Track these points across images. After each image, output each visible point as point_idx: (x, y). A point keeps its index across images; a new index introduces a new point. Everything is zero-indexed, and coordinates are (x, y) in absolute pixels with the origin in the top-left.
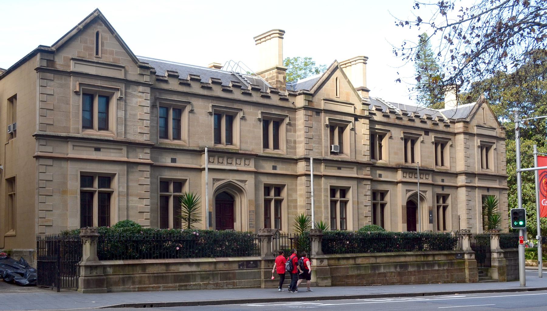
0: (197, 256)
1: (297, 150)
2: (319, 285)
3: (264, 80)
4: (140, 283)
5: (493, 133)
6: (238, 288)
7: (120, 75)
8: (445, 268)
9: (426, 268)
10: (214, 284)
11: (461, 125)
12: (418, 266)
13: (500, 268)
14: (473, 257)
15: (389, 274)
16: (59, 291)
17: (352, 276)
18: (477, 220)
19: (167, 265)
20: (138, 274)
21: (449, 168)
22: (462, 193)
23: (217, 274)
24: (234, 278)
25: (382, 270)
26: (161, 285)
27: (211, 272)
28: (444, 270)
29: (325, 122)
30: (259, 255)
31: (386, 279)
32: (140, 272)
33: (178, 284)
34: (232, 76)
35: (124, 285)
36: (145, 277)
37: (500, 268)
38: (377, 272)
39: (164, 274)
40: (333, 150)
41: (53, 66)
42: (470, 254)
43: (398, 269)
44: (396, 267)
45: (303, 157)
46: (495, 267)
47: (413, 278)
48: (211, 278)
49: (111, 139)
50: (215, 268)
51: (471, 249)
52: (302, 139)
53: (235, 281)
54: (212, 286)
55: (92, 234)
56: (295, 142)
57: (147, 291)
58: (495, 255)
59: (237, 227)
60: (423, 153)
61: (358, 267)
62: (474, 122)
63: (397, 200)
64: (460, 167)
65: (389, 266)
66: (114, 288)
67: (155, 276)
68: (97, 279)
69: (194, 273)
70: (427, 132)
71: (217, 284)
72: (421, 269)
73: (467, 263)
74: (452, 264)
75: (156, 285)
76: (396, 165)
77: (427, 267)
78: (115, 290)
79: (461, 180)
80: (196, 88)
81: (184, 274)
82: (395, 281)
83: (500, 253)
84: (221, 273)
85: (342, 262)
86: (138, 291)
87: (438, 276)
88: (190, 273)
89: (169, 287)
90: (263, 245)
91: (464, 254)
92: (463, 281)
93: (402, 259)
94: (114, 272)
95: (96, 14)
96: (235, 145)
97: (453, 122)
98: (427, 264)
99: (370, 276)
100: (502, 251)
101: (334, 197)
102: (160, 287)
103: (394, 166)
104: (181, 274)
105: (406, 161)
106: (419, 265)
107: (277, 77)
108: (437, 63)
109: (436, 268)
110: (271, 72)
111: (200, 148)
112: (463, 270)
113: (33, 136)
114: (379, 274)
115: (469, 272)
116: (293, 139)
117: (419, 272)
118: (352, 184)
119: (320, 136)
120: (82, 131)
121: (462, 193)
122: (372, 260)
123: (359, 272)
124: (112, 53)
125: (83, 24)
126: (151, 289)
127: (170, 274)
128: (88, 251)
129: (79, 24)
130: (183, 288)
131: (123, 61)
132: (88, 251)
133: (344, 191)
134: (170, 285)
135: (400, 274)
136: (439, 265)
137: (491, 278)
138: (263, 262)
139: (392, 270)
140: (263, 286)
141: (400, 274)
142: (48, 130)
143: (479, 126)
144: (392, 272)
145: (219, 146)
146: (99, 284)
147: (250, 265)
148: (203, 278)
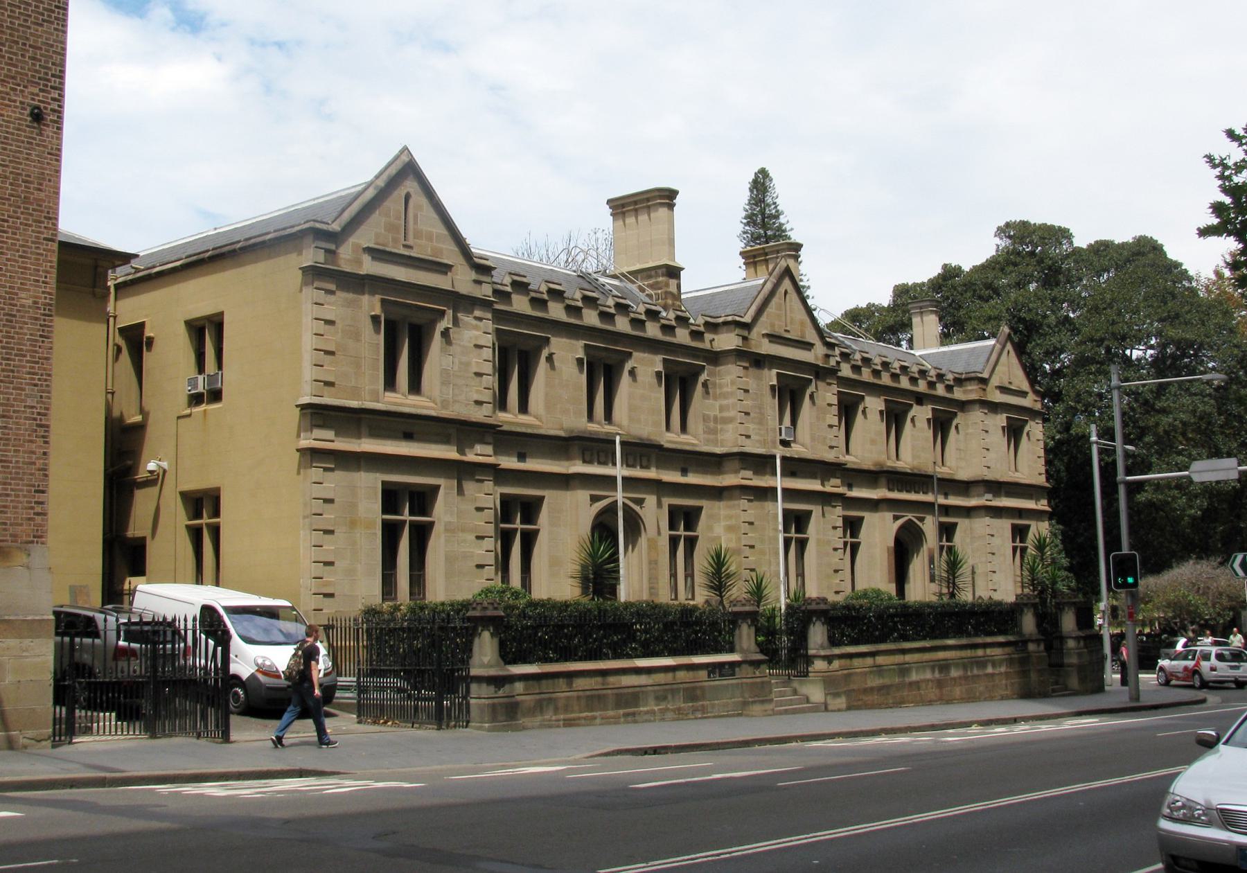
4: (567, 709)
8: (1003, 669)
9: (975, 672)
10: (674, 711)
12: (965, 667)
14: (1042, 647)
15: (923, 685)
16: (439, 728)
17: (872, 689)
19: (604, 673)
20: (561, 691)
23: (678, 689)
24: (703, 698)
25: (914, 677)
26: (596, 714)
30: (732, 650)
32: (564, 688)
33: (621, 712)
34: (580, 280)
38: (907, 680)
41: (334, 263)
43: (937, 675)
46: (1070, 665)
47: (958, 691)
48: (670, 697)
49: (433, 413)
55: (496, 613)
58: (1071, 644)
60: (639, 405)
61: (879, 670)
62: (995, 381)
63: (565, 524)
65: (924, 667)
66: (523, 721)
67: (588, 697)
70: (920, 399)
71: (679, 709)
76: (875, 465)
78: (530, 725)
80: (556, 311)
81: (630, 690)
83: (1077, 639)
84: (684, 689)
85: (857, 662)
86: (565, 726)
93: (941, 655)
94: (526, 688)
95: (405, 158)
97: (713, 327)
98: (977, 662)
99: (900, 687)
100: (1081, 634)
101: (396, 511)
102: (595, 718)
103: (872, 468)
104: (626, 691)
109: (990, 670)
111: (565, 431)
114: (911, 684)
117: (966, 678)
118: (446, 486)
122: (898, 658)
124: (430, 237)
125: (385, 177)
129: (377, 177)
130: (630, 719)
131: (449, 254)
133: (422, 500)
134: (611, 713)
135: (940, 684)
136: (994, 666)
137: (1066, 689)
141: (940, 684)
142: (326, 394)
143: (774, 338)
145: (503, 416)
147: (724, 671)
148: (660, 698)
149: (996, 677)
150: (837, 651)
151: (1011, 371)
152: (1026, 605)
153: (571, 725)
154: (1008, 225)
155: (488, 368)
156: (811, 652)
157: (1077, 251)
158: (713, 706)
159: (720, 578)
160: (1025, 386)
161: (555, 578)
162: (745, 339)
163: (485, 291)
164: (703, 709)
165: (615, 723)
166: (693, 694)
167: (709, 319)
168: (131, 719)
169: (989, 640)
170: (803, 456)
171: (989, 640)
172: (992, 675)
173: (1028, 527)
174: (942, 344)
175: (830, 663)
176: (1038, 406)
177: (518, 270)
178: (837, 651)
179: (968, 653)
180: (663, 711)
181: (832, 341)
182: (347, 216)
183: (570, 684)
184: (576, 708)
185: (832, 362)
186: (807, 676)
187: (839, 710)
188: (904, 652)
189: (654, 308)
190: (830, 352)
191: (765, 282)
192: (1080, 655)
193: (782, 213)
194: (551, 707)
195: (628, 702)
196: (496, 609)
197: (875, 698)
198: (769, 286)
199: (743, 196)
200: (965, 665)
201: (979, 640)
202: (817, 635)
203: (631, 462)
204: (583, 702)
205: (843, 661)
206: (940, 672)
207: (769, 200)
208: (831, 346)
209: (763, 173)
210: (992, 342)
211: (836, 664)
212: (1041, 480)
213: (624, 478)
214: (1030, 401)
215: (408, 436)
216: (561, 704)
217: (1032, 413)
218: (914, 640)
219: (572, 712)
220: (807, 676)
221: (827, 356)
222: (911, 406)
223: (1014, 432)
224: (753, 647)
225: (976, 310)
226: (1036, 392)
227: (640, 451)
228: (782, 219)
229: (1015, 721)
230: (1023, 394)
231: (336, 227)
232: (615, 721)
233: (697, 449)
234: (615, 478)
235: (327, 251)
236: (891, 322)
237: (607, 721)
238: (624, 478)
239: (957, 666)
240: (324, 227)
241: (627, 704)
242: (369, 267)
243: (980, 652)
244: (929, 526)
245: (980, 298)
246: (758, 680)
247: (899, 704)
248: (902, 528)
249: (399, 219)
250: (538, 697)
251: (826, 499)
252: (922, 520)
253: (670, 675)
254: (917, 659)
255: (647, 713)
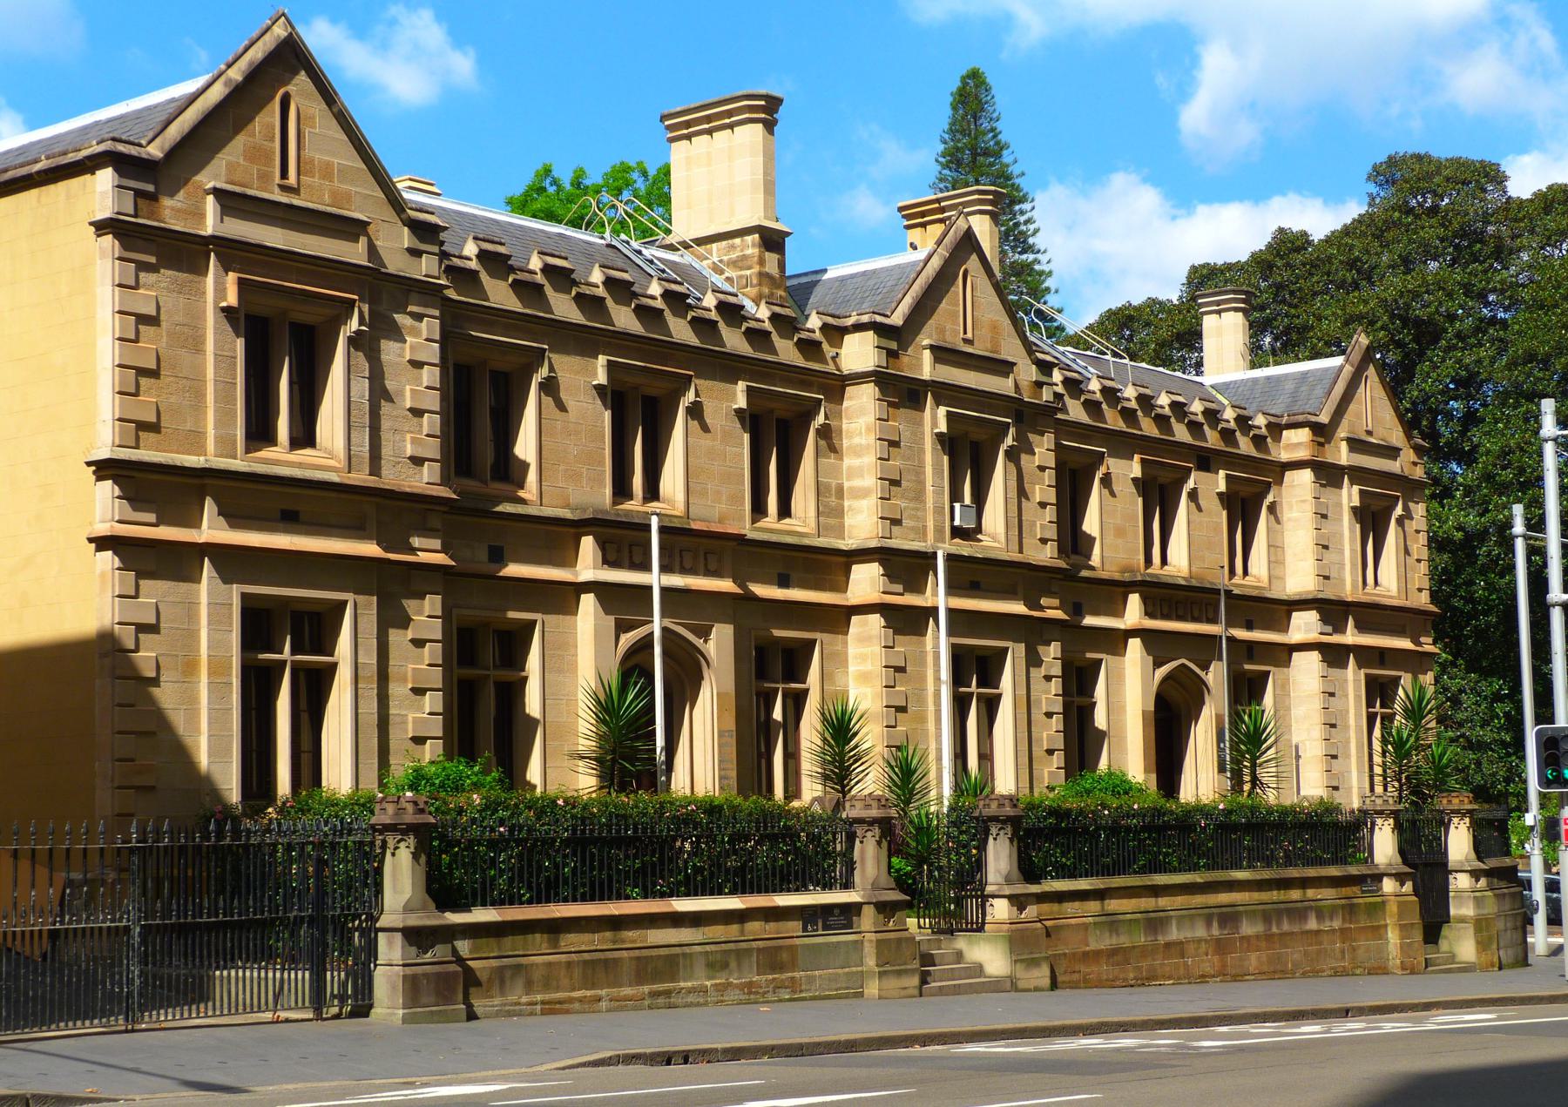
0: (693, 891)
1: (848, 521)
2: (1021, 985)
3: (704, 267)
4: (547, 985)
5: (1394, 466)
6: (804, 999)
7: (354, 253)
8: (1337, 924)
9: (1286, 927)
11: (1303, 435)
12: (1267, 917)
13: (1480, 924)
14: (1408, 887)
15: (1191, 948)
17: (1097, 954)
18: (1354, 759)
19: (616, 923)
20: (539, 954)
21: (1265, 583)
22: (1307, 667)
23: (748, 951)
24: (793, 966)
25: (1174, 934)
26: (603, 992)
27: (731, 946)
28: (1334, 931)
29: (935, 424)
30: (847, 885)
31: (1186, 964)
33: (646, 989)
35: (503, 994)
36: (559, 963)
37: (1480, 924)
38: (1161, 939)
39: (610, 955)
40: (957, 522)
42: (1400, 878)
43: (1215, 931)
44: (1208, 921)
45: (873, 544)
46: (1462, 920)
47: (1253, 960)
48: (733, 964)
49: (334, 478)
50: (742, 933)
51: (1399, 860)
52: (870, 481)
53: (796, 974)
54: (734, 995)
55: (421, 819)
56: (840, 492)
57: (567, 1012)
58: (1461, 882)
59: (680, 783)
60: (699, 471)
61: (1112, 923)
64: (1299, 579)
65: (1192, 917)
67: (585, 962)
68: (438, 974)
69: (687, 950)
71: (750, 984)
72: (1274, 930)
73: (1392, 908)
74: (1350, 910)
75: (589, 993)
77: (1291, 921)
79: (1305, 626)
82: (1208, 970)
83: (1475, 874)
84: (759, 950)
85: (1071, 907)
86: (543, 1013)
87: (1319, 952)
88: (678, 950)
89: (626, 999)
90: (862, 852)
91: (1378, 878)
92: (1381, 970)
93: (1224, 898)
95: (280, 31)
96: (671, 502)
99: (1144, 952)
103: (1117, 576)
104: (655, 952)
105: (1148, 561)
106: (1269, 915)
107: (762, 262)
108: (1017, 181)
109: (1312, 924)
110: (737, 241)
112: (1378, 931)
113: (89, 464)
114: (1168, 945)
115: (1402, 938)
116: (834, 483)
119: (919, 471)
120: (248, 451)
121: (1307, 667)
123: (1114, 941)
124: (327, 172)
125: (243, 64)
126: (577, 1005)
127: (625, 954)
128: (400, 877)
130: (661, 1000)
131: (363, 203)
132: (400, 877)
134: (628, 991)
135: (1221, 947)
136: (1320, 917)
138: (869, 913)
139: (1200, 932)
140: (872, 988)
144: (1200, 941)
146: (449, 990)
148: (717, 964)
149: (1325, 938)
150: (1034, 889)
151: (1374, 412)
152: (1380, 813)
153: (552, 1012)
154: (1392, 162)
155: (433, 401)
156: (989, 889)
157: (1513, 208)
158: (811, 980)
159: (842, 762)
160: (1396, 437)
161: (564, 766)
162: (892, 354)
163: (426, 268)
164: (793, 985)
165: (635, 1009)
166: (775, 959)
167: (830, 320)
168: (193, 1001)
169: (1312, 872)
170: (992, 555)
171: (1312, 872)
172: (1318, 932)
173: (1396, 681)
174: (1253, 366)
175: (1021, 909)
176: (1419, 473)
177: (497, 234)
178: (1034, 889)
179: (1274, 895)
180: (722, 988)
181: (1048, 358)
182: (175, 131)
183: (555, 943)
184: (565, 982)
185: (1046, 395)
186: (980, 929)
187: (1036, 989)
188: (1156, 891)
189: (732, 299)
190: (1044, 379)
191: (930, 257)
192: (1478, 902)
193: (1007, 146)
194: (520, 984)
195: (660, 969)
196: (422, 811)
197: (1104, 969)
198: (936, 263)
199: (941, 115)
200: (1269, 915)
201: (1293, 873)
202: (999, 858)
203: (612, 557)
204: (577, 972)
205: (1046, 907)
206: (1222, 925)
207: (986, 125)
208: (1046, 367)
209: (975, 76)
210: (1338, 361)
211: (1031, 911)
212: (1423, 600)
213: (665, 591)
214: (1407, 463)
215: (290, 520)
216: (537, 975)
217: (1408, 487)
218: (1175, 870)
219: (558, 989)
220: (980, 929)
221: (1039, 385)
222: (1190, 470)
223: (1372, 521)
224: (886, 880)
225: (1327, 313)
226: (1418, 450)
227: (687, 546)
228: (1007, 157)
229: (1345, 1013)
230: (1392, 452)
231: (155, 151)
232: (636, 1003)
233: (806, 542)
234: (649, 588)
235: (139, 194)
236: (1166, 333)
237: (620, 1004)
238: (665, 591)
239: (1251, 915)
240: (133, 151)
241: (656, 977)
242: (211, 222)
243: (1295, 894)
244: (1216, 676)
245: (1341, 285)
246: (892, 935)
247: (1146, 980)
248: (1166, 679)
249: (272, 139)
250: (494, 963)
251: (1032, 632)
252: (704, 633)
253: (735, 928)
254: (1182, 909)
255: (690, 991)
